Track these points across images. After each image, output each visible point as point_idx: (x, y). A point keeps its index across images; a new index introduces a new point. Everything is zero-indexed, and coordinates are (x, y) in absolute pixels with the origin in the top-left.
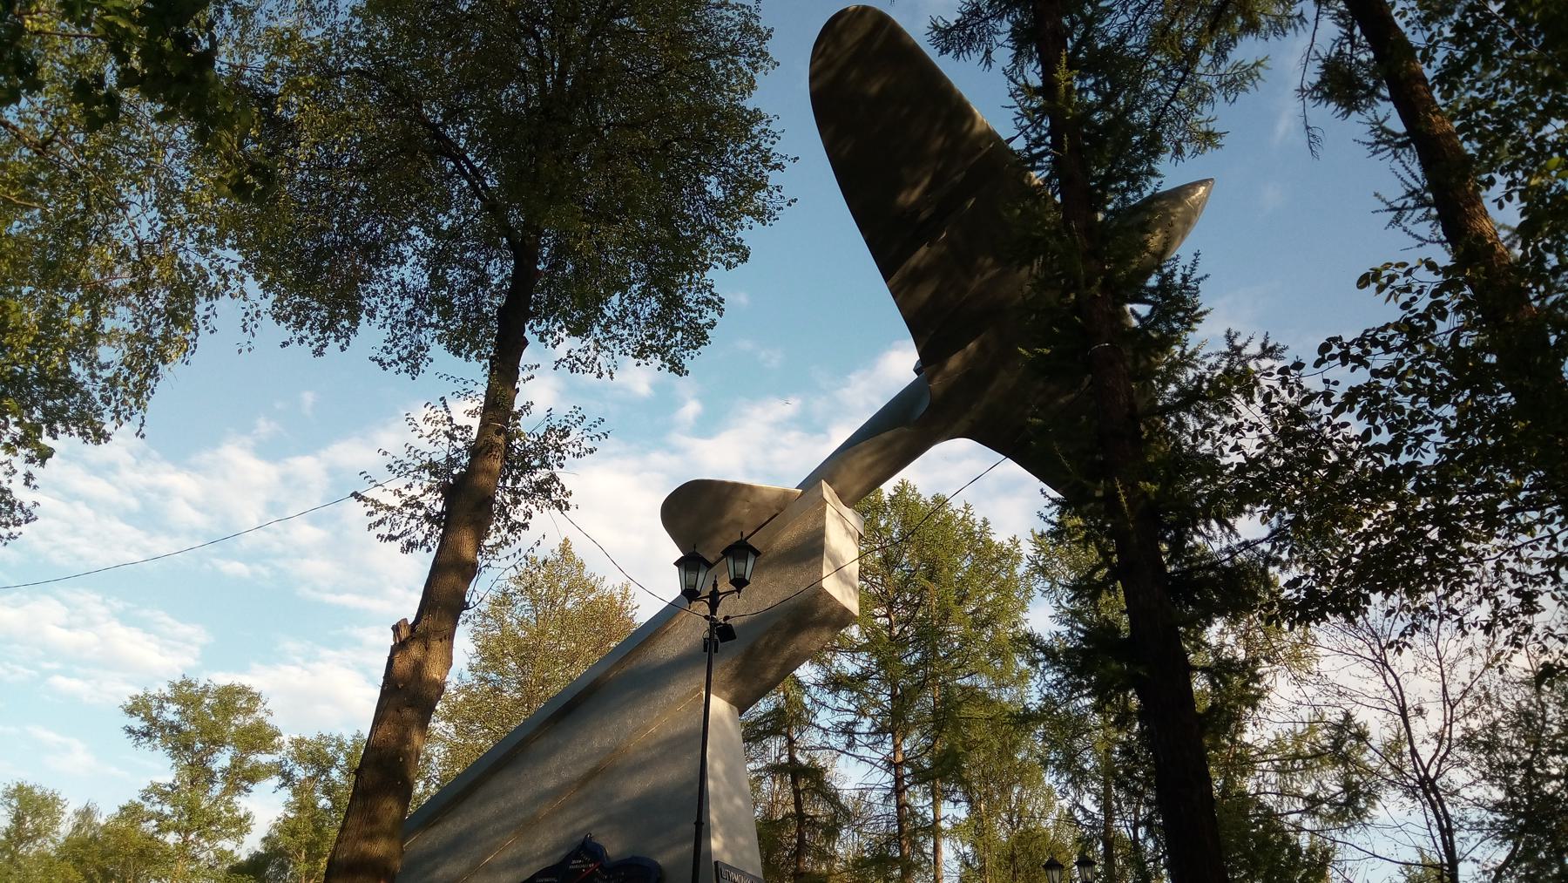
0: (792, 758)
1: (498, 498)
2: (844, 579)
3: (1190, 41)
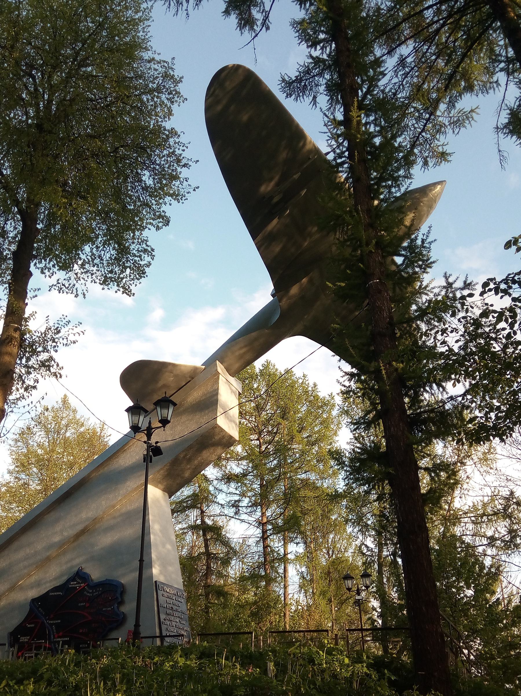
0: (203, 521)
1: (17, 371)
2: (230, 419)
3: (434, 95)
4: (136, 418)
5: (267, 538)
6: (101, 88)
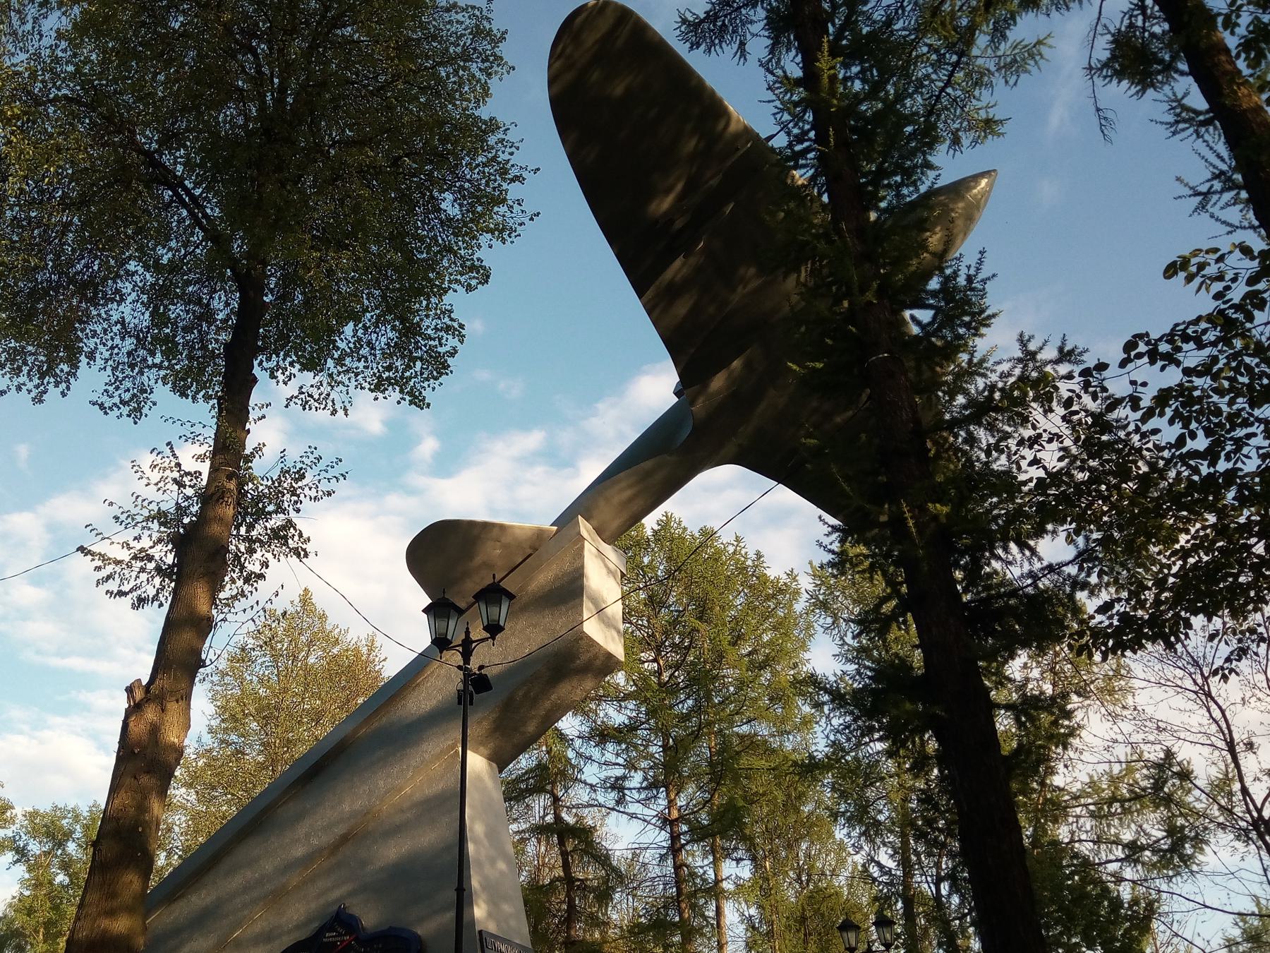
0: (558, 818)
1: (232, 547)
2: (607, 623)
3: (964, 22)
4: (442, 624)
5: (680, 850)
6: (368, 59)
